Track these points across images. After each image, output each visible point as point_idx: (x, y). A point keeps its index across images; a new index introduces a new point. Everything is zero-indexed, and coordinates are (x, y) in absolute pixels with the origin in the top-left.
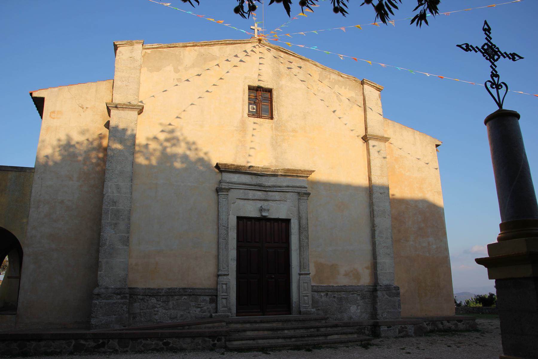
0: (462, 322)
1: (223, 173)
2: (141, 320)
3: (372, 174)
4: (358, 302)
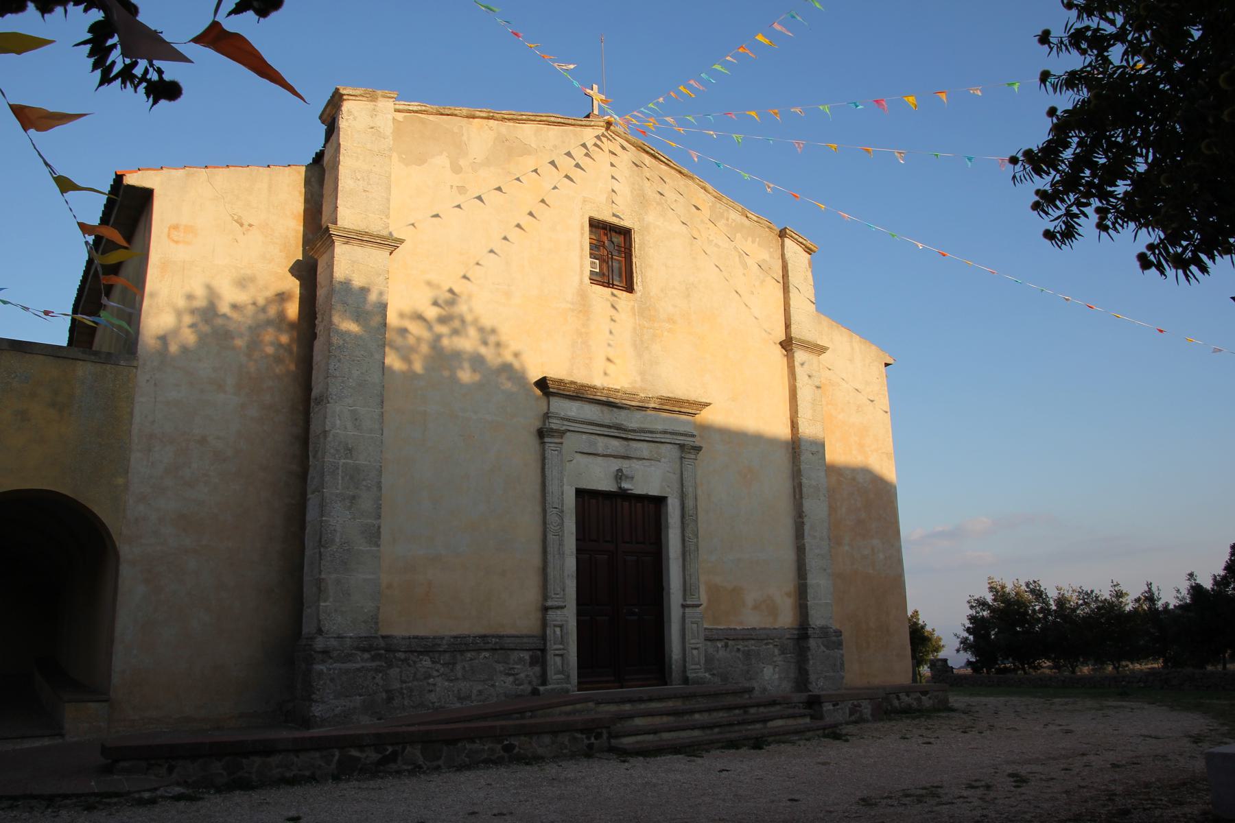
0: (928, 696)
1: (551, 398)
2: (403, 705)
3: (799, 416)
4: (775, 659)
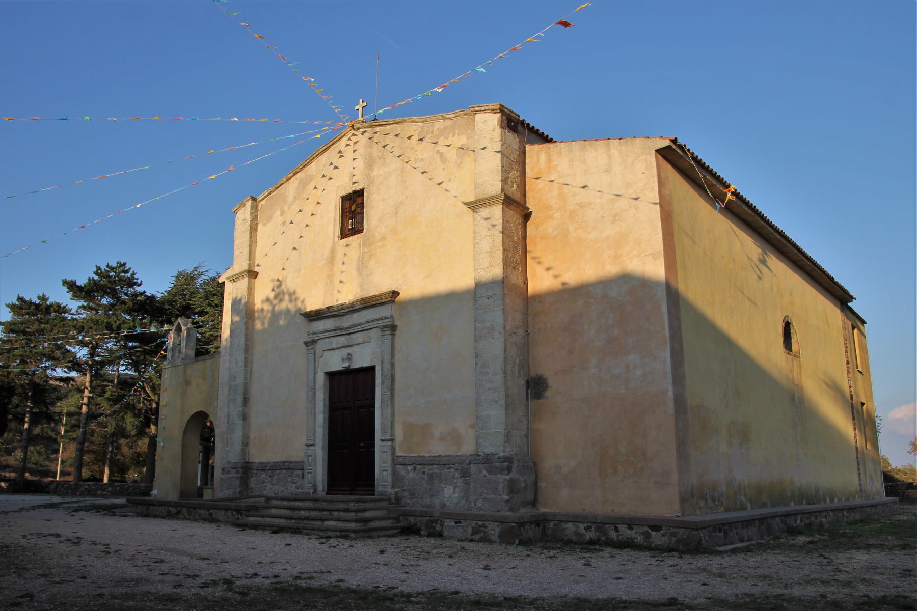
4: (455, 481)
